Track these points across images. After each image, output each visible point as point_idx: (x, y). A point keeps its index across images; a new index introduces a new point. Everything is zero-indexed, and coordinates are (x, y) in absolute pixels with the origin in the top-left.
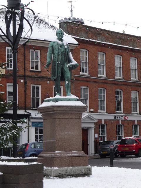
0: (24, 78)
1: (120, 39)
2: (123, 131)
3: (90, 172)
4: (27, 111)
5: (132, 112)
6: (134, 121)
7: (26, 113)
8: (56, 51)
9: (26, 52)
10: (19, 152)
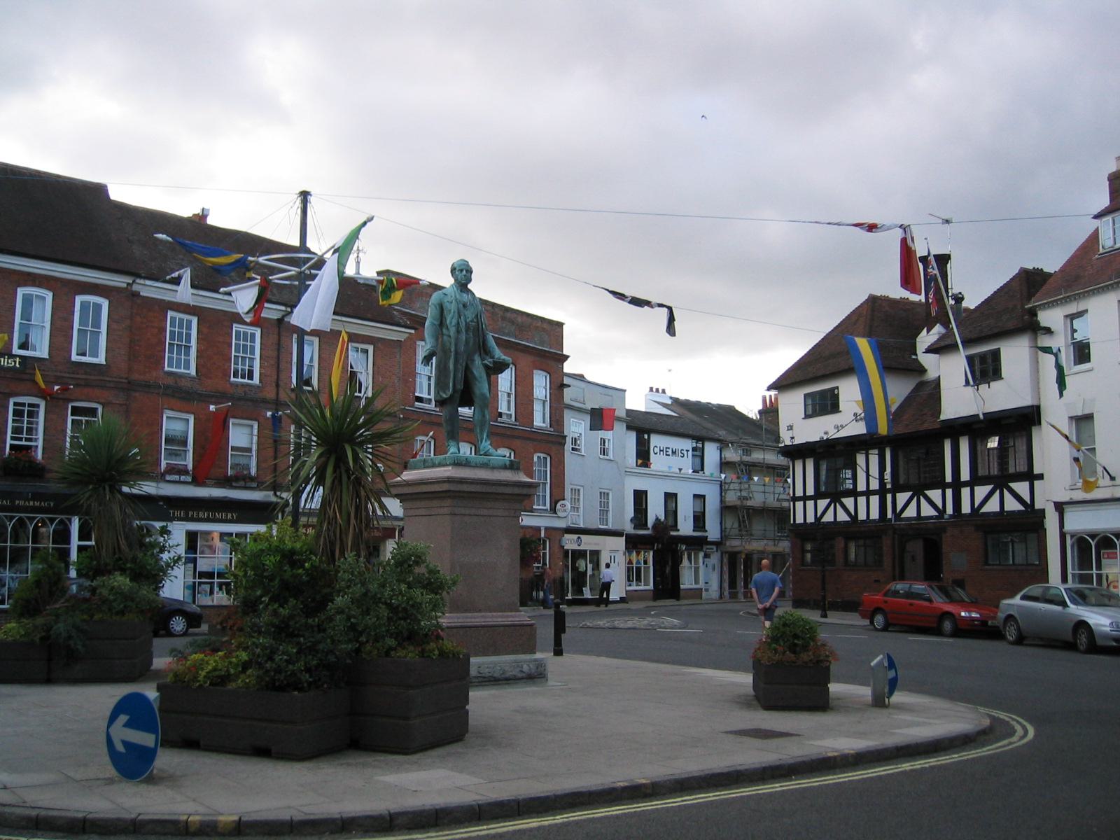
0: (274, 407)
1: (512, 322)
2: (548, 554)
3: (542, 669)
4: (278, 493)
5: (534, 507)
6: (538, 529)
7: (274, 499)
8: (450, 320)
9: (283, 339)
10: (776, 617)
